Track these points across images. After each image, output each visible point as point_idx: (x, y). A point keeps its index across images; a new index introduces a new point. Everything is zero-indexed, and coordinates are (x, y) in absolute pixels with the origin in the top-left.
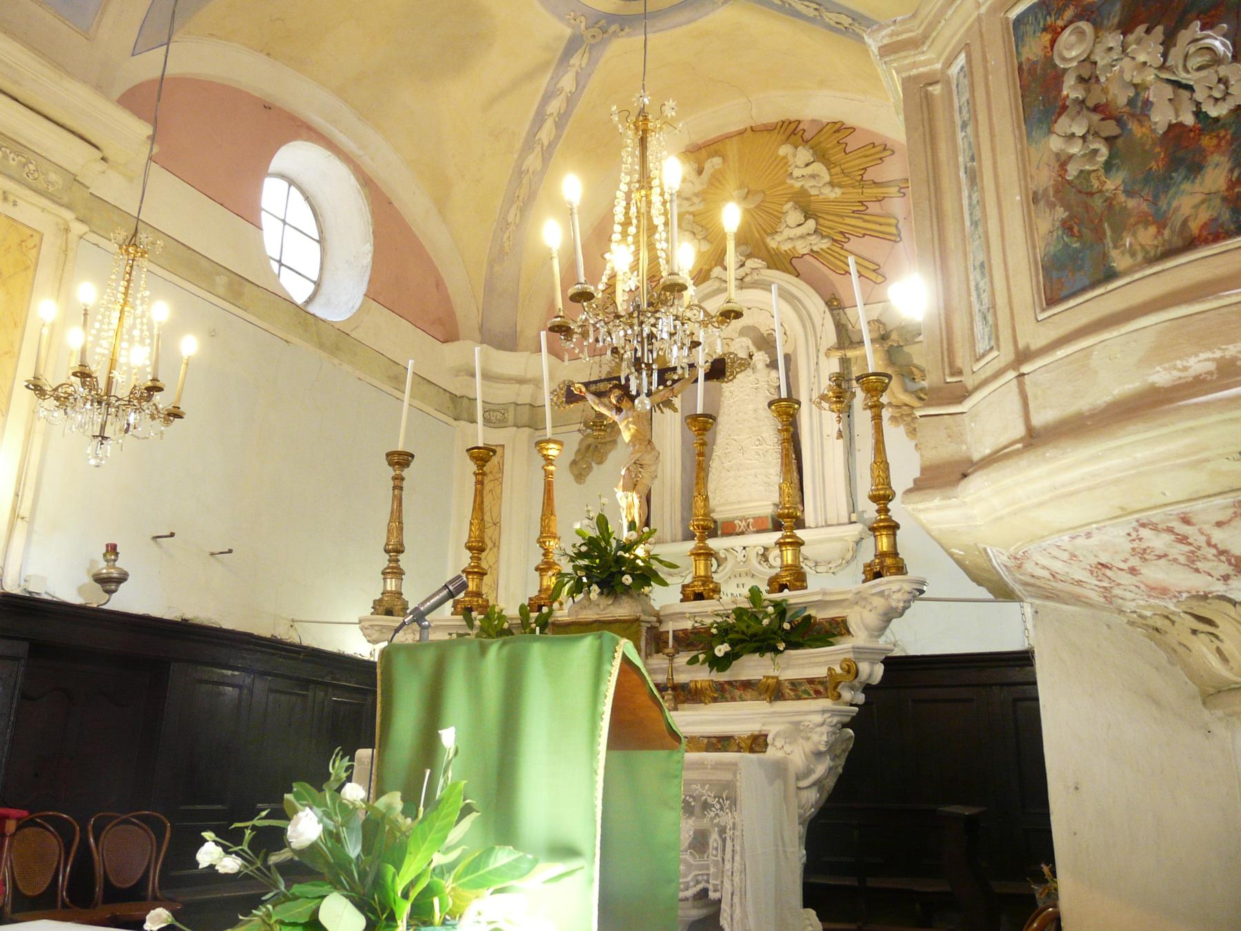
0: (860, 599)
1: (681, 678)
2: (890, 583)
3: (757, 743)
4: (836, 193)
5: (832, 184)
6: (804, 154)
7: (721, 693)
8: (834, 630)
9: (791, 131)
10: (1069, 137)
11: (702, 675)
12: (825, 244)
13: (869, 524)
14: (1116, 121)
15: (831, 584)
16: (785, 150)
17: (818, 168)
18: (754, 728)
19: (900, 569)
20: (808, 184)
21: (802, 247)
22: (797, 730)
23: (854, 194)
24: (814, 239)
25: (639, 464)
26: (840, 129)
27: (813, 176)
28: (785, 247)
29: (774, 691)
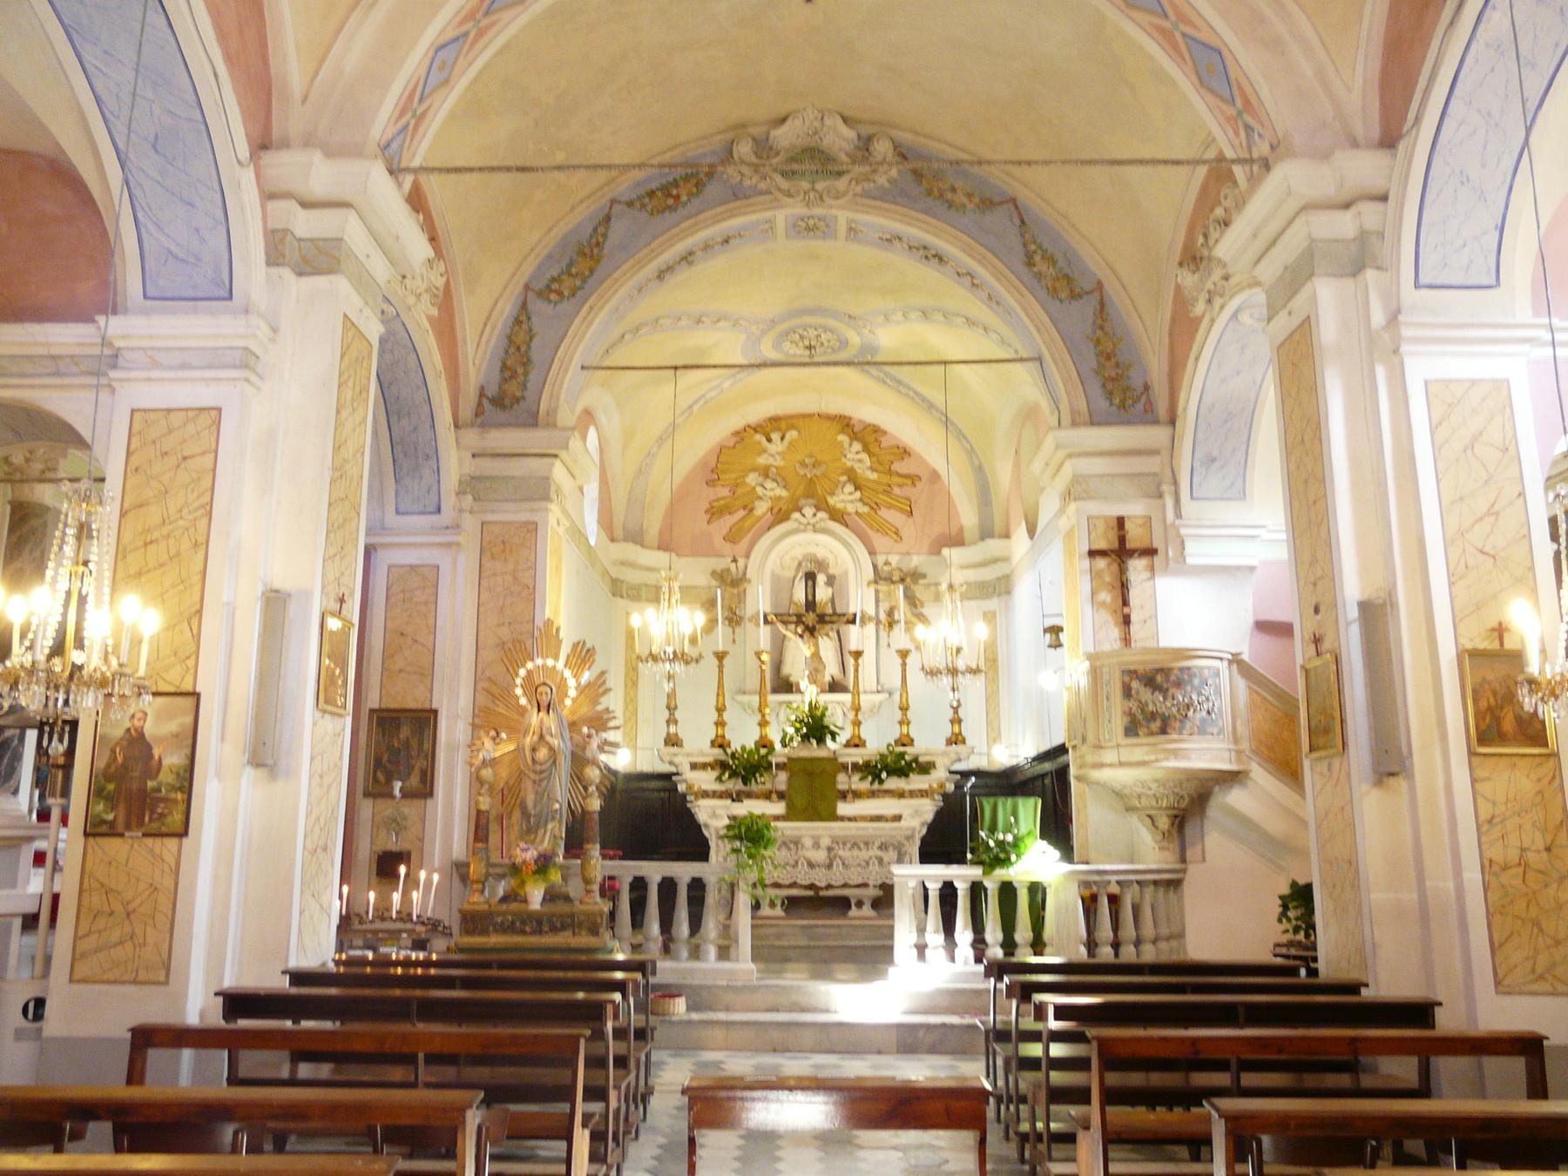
0: (944, 754)
1: (854, 787)
2: (959, 748)
3: (898, 818)
4: (874, 476)
5: (872, 469)
6: (857, 446)
7: (873, 794)
8: (926, 768)
9: (845, 423)
10: (1133, 705)
11: (864, 786)
12: (866, 509)
13: (812, 641)
14: (1143, 706)
15: (928, 741)
16: (843, 438)
17: (864, 456)
18: (896, 811)
19: (964, 742)
20: (856, 466)
21: (850, 508)
22: (916, 813)
23: (885, 479)
24: (859, 505)
25: (816, 670)
26: (877, 430)
27: (860, 461)
28: (840, 506)
29: (901, 795)
